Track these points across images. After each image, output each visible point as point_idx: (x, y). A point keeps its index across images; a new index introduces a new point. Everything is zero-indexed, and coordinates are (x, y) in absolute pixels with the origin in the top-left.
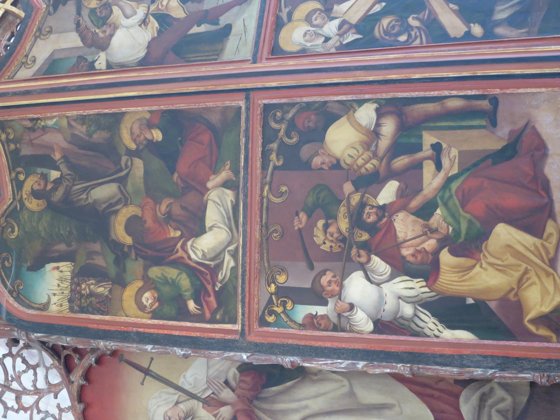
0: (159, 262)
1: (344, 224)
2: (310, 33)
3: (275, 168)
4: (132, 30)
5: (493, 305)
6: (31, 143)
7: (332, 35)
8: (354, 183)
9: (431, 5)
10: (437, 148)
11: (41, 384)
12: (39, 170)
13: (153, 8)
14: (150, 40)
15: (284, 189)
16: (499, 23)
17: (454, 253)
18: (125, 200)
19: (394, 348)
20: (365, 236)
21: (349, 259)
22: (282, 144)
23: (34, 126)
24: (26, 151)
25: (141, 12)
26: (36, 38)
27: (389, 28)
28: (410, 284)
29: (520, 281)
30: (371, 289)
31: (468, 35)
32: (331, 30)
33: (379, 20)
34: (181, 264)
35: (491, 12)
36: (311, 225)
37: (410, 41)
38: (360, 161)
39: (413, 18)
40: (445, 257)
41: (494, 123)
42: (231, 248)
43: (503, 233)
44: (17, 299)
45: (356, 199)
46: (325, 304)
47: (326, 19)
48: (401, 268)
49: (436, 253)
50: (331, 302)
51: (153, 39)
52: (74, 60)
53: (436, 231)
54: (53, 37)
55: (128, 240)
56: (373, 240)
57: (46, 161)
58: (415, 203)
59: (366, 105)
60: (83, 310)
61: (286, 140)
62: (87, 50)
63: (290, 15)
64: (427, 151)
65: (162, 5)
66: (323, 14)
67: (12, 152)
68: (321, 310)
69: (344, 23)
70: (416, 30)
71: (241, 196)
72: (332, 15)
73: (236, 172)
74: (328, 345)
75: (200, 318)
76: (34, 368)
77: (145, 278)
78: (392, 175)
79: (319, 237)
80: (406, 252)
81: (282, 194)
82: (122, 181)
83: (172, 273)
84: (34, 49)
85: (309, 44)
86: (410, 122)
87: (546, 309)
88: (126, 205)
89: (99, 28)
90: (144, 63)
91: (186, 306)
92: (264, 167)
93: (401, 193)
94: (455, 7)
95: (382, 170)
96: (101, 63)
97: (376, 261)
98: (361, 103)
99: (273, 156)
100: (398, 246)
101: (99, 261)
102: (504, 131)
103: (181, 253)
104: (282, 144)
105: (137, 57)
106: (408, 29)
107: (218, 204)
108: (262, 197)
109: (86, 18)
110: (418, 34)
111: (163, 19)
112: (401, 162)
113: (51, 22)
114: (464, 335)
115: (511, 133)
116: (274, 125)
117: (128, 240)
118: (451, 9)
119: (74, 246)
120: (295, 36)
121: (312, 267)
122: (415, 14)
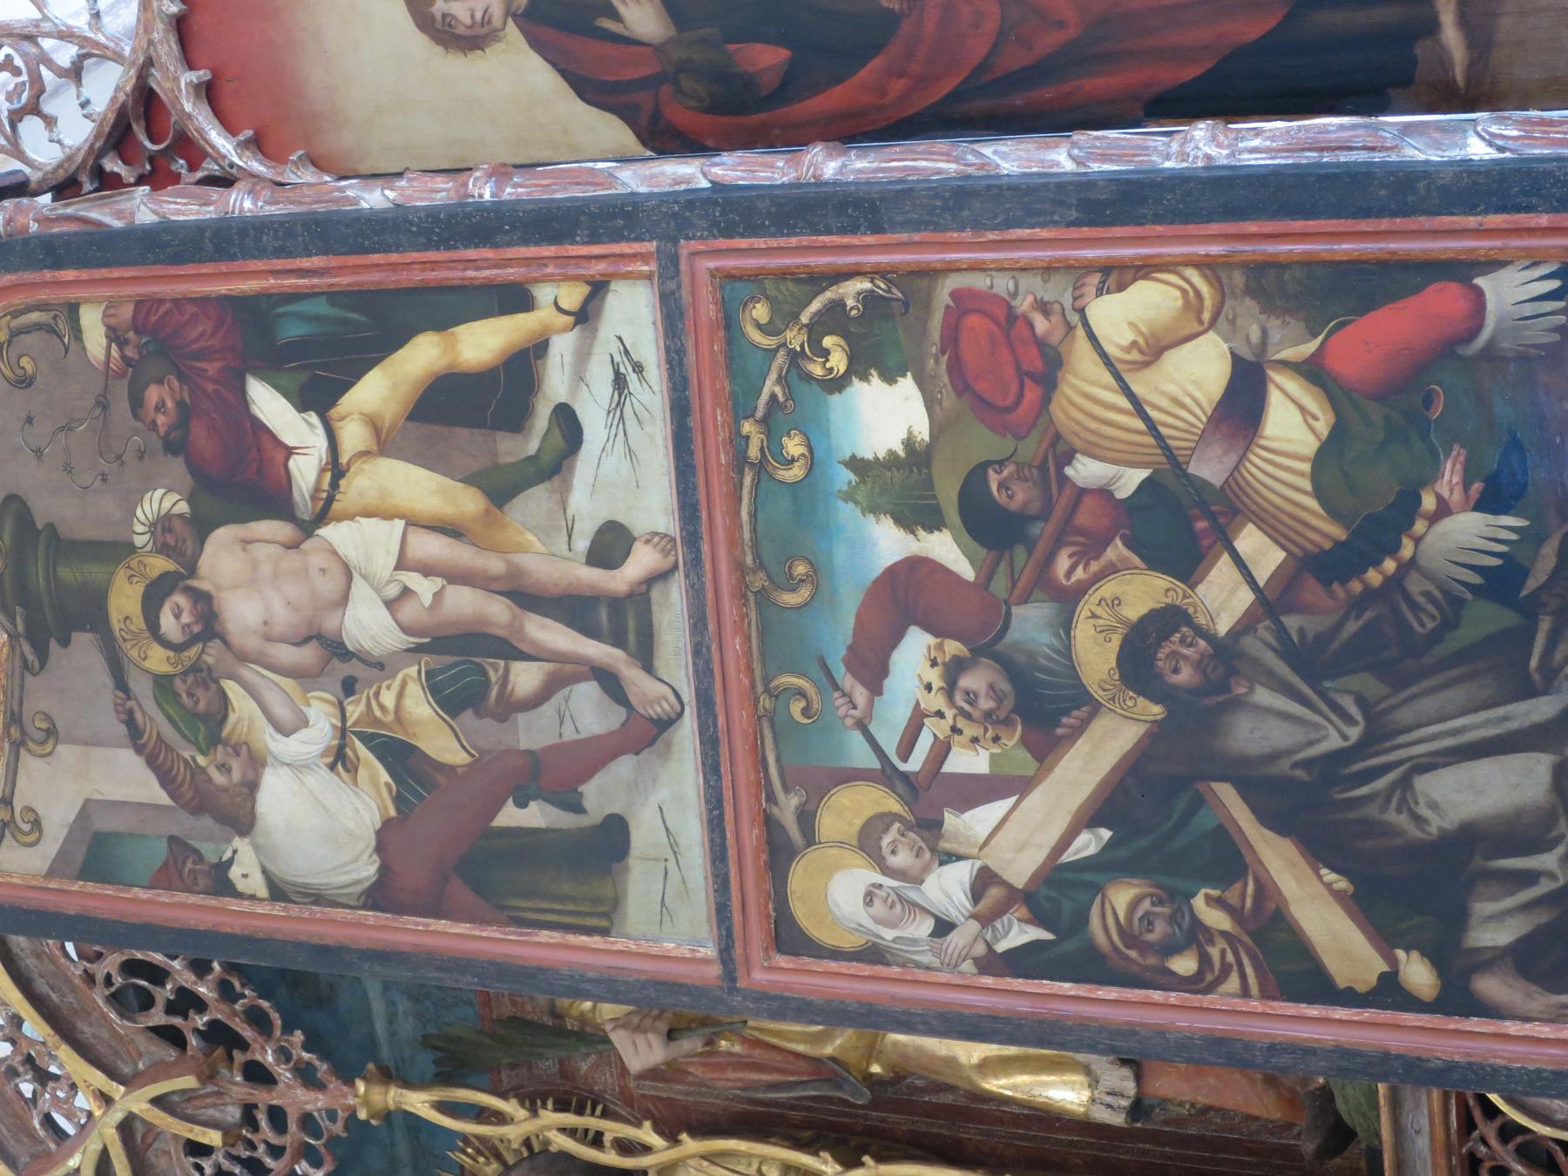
2: (881, 893)
4: (310, 780)
7: (954, 915)
9: (1261, 863)
13: (355, 711)
14: (378, 826)
16: (1489, 961)
27: (1136, 923)
31: (1390, 993)
32: (949, 897)
33: (1098, 889)
35: (1458, 919)
37: (1209, 978)
39: (1208, 898)
47: (927, 855)
51: (387, 824)
52: (160, 850)
54: (66, 752)
63: (807, 819)
65: (382, 708)
66: (912, 835)
69: (984, 880)
70: (1221, 944)
72: (945, 845)
84: (21, 783)
85: (888, 934)
89: (204, 753)
94: (1342, 884)
96: (246, 872)
105: (355, 876)
106: (1197, 936)
109: (150, 707)
110: (1230, 957)
111: (398, 755)
113: (41, 699)
118: (1328, 886)
122: (1214, 888)
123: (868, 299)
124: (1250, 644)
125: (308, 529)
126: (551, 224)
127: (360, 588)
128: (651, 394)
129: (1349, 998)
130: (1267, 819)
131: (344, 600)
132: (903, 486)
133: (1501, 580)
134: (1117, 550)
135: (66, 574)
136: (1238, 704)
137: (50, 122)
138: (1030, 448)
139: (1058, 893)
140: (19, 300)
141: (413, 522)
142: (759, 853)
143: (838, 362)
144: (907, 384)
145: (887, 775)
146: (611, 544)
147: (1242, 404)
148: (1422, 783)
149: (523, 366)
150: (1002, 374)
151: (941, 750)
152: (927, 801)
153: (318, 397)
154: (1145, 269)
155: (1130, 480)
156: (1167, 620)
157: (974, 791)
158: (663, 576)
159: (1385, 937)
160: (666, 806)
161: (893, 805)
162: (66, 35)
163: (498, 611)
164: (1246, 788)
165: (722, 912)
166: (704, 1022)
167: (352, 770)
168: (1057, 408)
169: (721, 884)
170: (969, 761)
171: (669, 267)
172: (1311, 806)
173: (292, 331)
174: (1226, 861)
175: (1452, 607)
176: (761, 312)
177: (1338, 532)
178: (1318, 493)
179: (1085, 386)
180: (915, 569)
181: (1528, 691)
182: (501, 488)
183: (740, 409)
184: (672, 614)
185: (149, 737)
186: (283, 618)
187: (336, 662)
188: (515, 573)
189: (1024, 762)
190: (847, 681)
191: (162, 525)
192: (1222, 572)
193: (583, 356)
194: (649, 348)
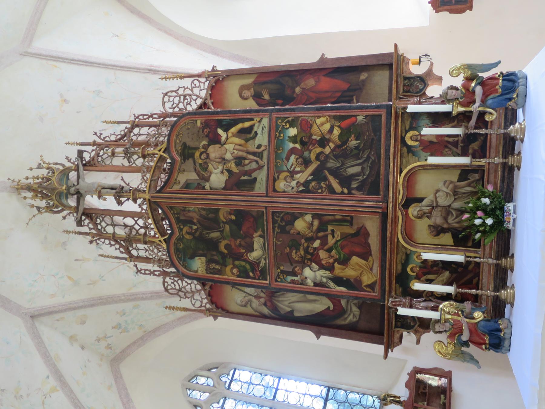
0: (238, 259)
1: (302, 252)
3: (277, 232)
4: (218, 175)
5: (352, 280)
6: (184, 215)
8: (305, 240)
10: (333, 231)
11: (193, 289)
12: (189, 225)
13: (225, 166)
15: (281, 239)
16: (353, 189)
17: (339, 264)
18: (224, 238)
19: (321, 292)
20: (310, 257)
21: (304, 263)
22: (279, 225)
23: (184, 210)
24: (182, 218)
25: (220, 168)
26: (179, 173)
28: (325, 272)
29: (361, 274)
30: (312, 273)
31: (342, 193)
33: (311, 183)
34: (246, 261)
35: (350, 184)
36: (291, 252)
38: (307, 233)
40: (336, 265)
41: (351, 224)
42: (264, 257)
43: (355, 259)
44: (185, 268)
45: (306, 245)
46: (297, 276)
48: (322, 267)
49: (333, 264)
50: (299, 276)
52: (196, 185)
53: (332, 257)
54: (185, 173)
55: (226, 252)
56: (312, 258)
57: (190, 222)
58: (326, 248)
59: (308, 215)
60: (211, 273)
61: (281, 224)
62: (201, 181)
63: (278, 177)
64: (329, 231)
67: (176, 218)
68: (296, 278)
69: (298, 182)
71: (266, 241)
73: (263, 232)
74: (299, 289)
75: (254, 278)
76: (190, 284)
77: (233, 264)
78: (318, 238)
79: (294, 256)
80: (323, 262)
81: (280, 241)
82: (222, 232)
83: (243, 263)
84: (179, 177)
86: (324, 222)
87: (369, 283)
88: (224, 240)
90: (224, 189)
91: (249, 274)
92: (274, 232)
93: (321, 244)
94: (338, 181)
95: (314, 236)
96: (207, 186)
97: (313, 264)
98: (306, 214)
99: (276, 228)
100: (321, 260)
101: (216, 258)
102: (355, 227)
103: (246, 257)
104: (279, 225)
106: (321, 187)
107: (258, 242)
108: (273, 242)
109: (198, 167)
111: (230, 172)
112: (321, 234)
113: (184, 167)
114: (343, 289)
115: (357, 228)
116: (276, 219)
117: (226, 252)
119: (205, 252)
120: (281, 185)
121: (292, 265)
123: (292, 120)
124: (330, 155)
125: (222, 145)
126: (257, 111)
127: (228, 152)
128: (266, 130)
129: (338, 194)
130: (331, 174)
131: (226, 153)
132: (294, 139)
133: (357, 148)
134: (317, 145)
135: (190, 151)
136: (329, 162)
137: (191, 106)
138: (308, 135)
139: (306, 184)
140: (190, 119)
141: (236, 144)
142: (272, 180)
143: (288, 126)
144: (295, 128)
145: (288, 171)
146: (259, 146)
147: (331, 131)
148: (347, 170)
149: (252, 127)
150: (306, 127)
151: (295, 168)
152: (292, 174)
153: (226, 130)
154: (322, 116)
155: (318, 138)
156: (321, 153)
157: (298, 172)
158: (264, 150)
159: (342, 186)
160: (262, 176)
161: (288, 174)
162: (196, 95)
163: (244, 154)
164: (328, 171)
165: (267, 187)
166: (195, 376)
167: (223, 173)
168: (311, 131)
169: (267, 184)
170: (298, 169)
171: (271, 115)
172: (335, 173)
173: (224, 123)
174: (325, 179)
175: (352, 150)
176: (280, 121)
177: (340, 143)
178: (339, 139)
179: (315, 128)
180: (294, 149)
181: (359, 159)
182: (247, 140)
183: (276, 131)
184: (265, 154)
185: (197, 171)
186: (218, 156)
187: (223, 160)
188: (247, 150)
189: (304, 169)
190: (285, 161)
191: (204, 145)
192: (328, 147)
193: (259, 126)
194: (267, 125)
